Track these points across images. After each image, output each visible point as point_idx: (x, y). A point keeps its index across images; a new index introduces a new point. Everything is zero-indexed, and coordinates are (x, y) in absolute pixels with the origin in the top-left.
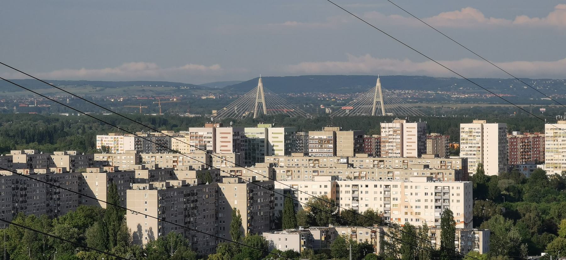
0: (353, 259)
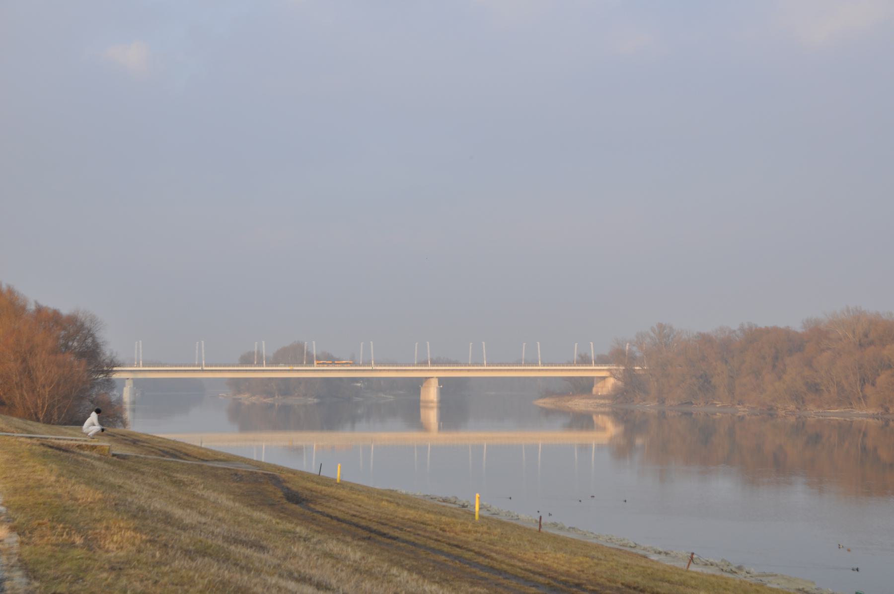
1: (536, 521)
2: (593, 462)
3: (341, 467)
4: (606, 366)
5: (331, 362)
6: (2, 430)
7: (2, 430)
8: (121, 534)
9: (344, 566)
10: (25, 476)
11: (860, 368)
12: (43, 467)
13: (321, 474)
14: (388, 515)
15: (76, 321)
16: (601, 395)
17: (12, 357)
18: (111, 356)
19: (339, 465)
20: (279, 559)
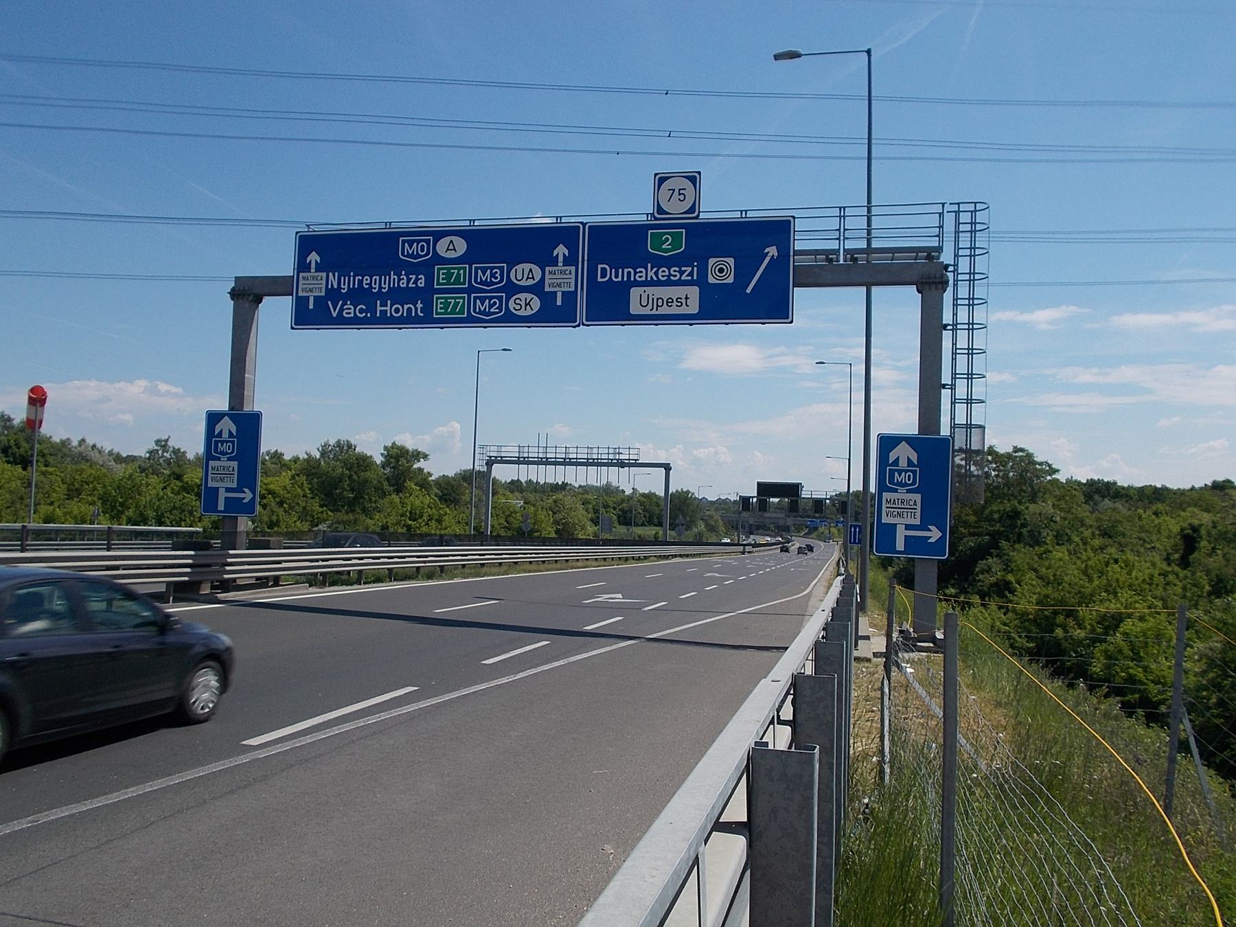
0: (1224, 924)
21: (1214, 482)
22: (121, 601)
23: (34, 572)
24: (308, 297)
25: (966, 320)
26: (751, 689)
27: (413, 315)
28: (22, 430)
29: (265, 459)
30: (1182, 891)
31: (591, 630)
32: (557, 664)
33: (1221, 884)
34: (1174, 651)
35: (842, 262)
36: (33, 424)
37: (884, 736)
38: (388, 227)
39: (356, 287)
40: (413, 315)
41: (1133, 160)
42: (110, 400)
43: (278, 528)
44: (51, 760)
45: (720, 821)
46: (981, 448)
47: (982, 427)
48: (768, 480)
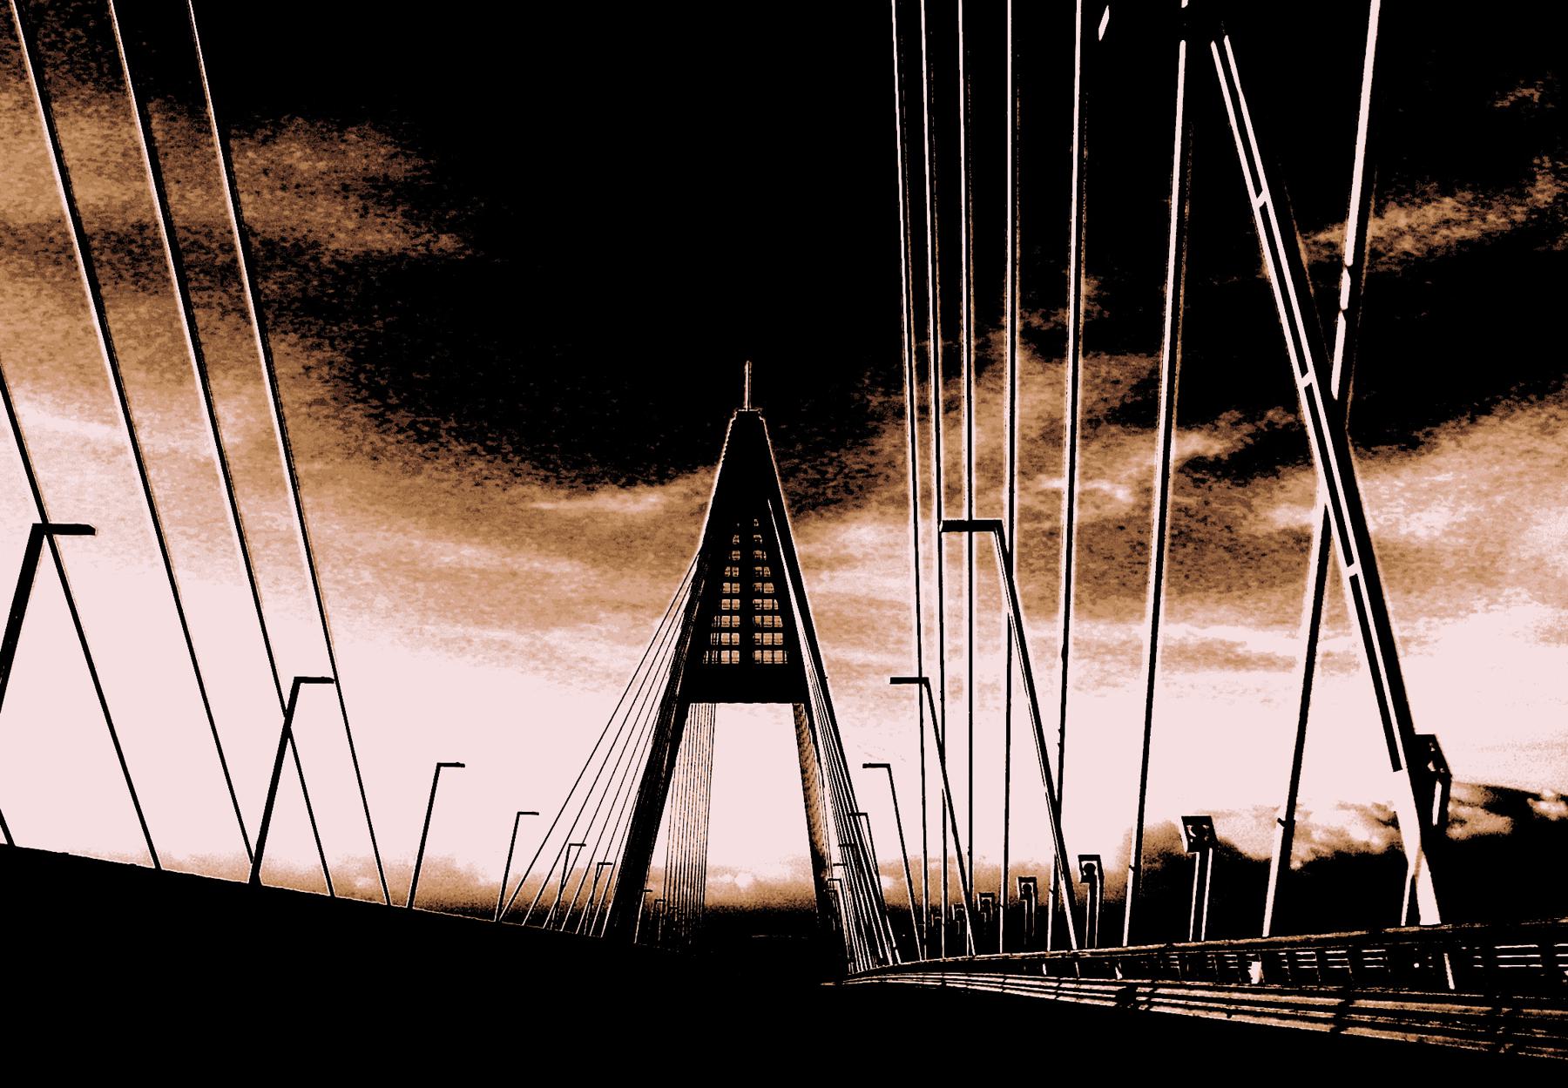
1: (223, 396)
2: (1447, 962)
3: (1021, 234)
4: (548, 501)
5: (1439, 787)
6: (2, 302)
7: (2, 302)
8: (132, 241)
9: (172, 355)
10: (99, 147)
11: (365, 169)
12: (1519, 490)
13: (974, 518)
14: (1343, 633)
15: (846, 509)
16: (159, 164)
17: (185, 211)
18: (474, 452)
19: (1183, 44)
20: (332, 547)
21: (1432, 739)
22: (1220, 487)
23: (447, 903)
24: (1129, 945)
25: (911, 668)
26: (74, 265)
27: (1227, 41)
28: (1387, 201)
29: (255, 152)
30: (1468, 567)
31: (1335, 557)
32: (1212, 942)
33: (91, 74)
34: (288, 245)
35: (891, 964)
36: (773, 661)
37: (1281, 995)
38: (778, 621)
39: (1213, 46)
40: (1227, 41)
41: (873, 850)
42: (1113, 559)
43: (93, 239)
44: (1374, 72)
45: (1296, 865)
46: (39, 521)
47: (866, 814)
48: (807, 584)
